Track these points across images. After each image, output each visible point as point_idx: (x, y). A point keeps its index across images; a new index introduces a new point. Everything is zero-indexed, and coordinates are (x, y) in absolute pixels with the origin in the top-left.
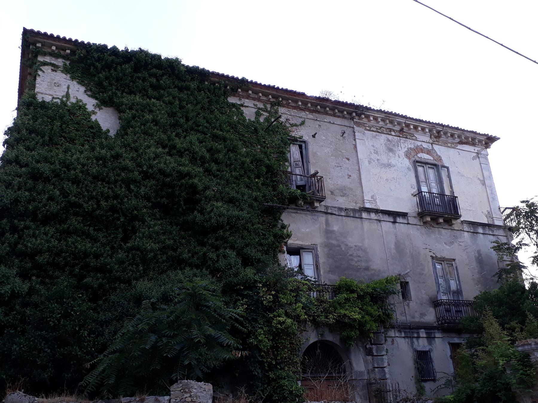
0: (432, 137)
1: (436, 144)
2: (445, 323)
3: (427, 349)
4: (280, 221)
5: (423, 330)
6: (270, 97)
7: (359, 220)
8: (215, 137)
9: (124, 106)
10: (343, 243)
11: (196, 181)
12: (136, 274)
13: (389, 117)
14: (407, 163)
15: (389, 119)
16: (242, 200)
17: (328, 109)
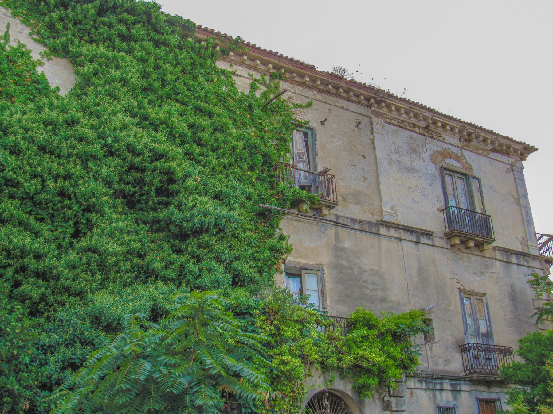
0: (462, 139)
1: (465, 149)
2: (475, 373)
4: (277, 230)
5: (447, 381)
6: (270, 66)
7: (375, 236)
8: (199, 110)
9: (83, 58)
11: (174, 164)
12: (91, 284)
13: (414, 109)
14: (433, 169)
15: (413, 112)
16: (233, 196)
17: (341, 90)
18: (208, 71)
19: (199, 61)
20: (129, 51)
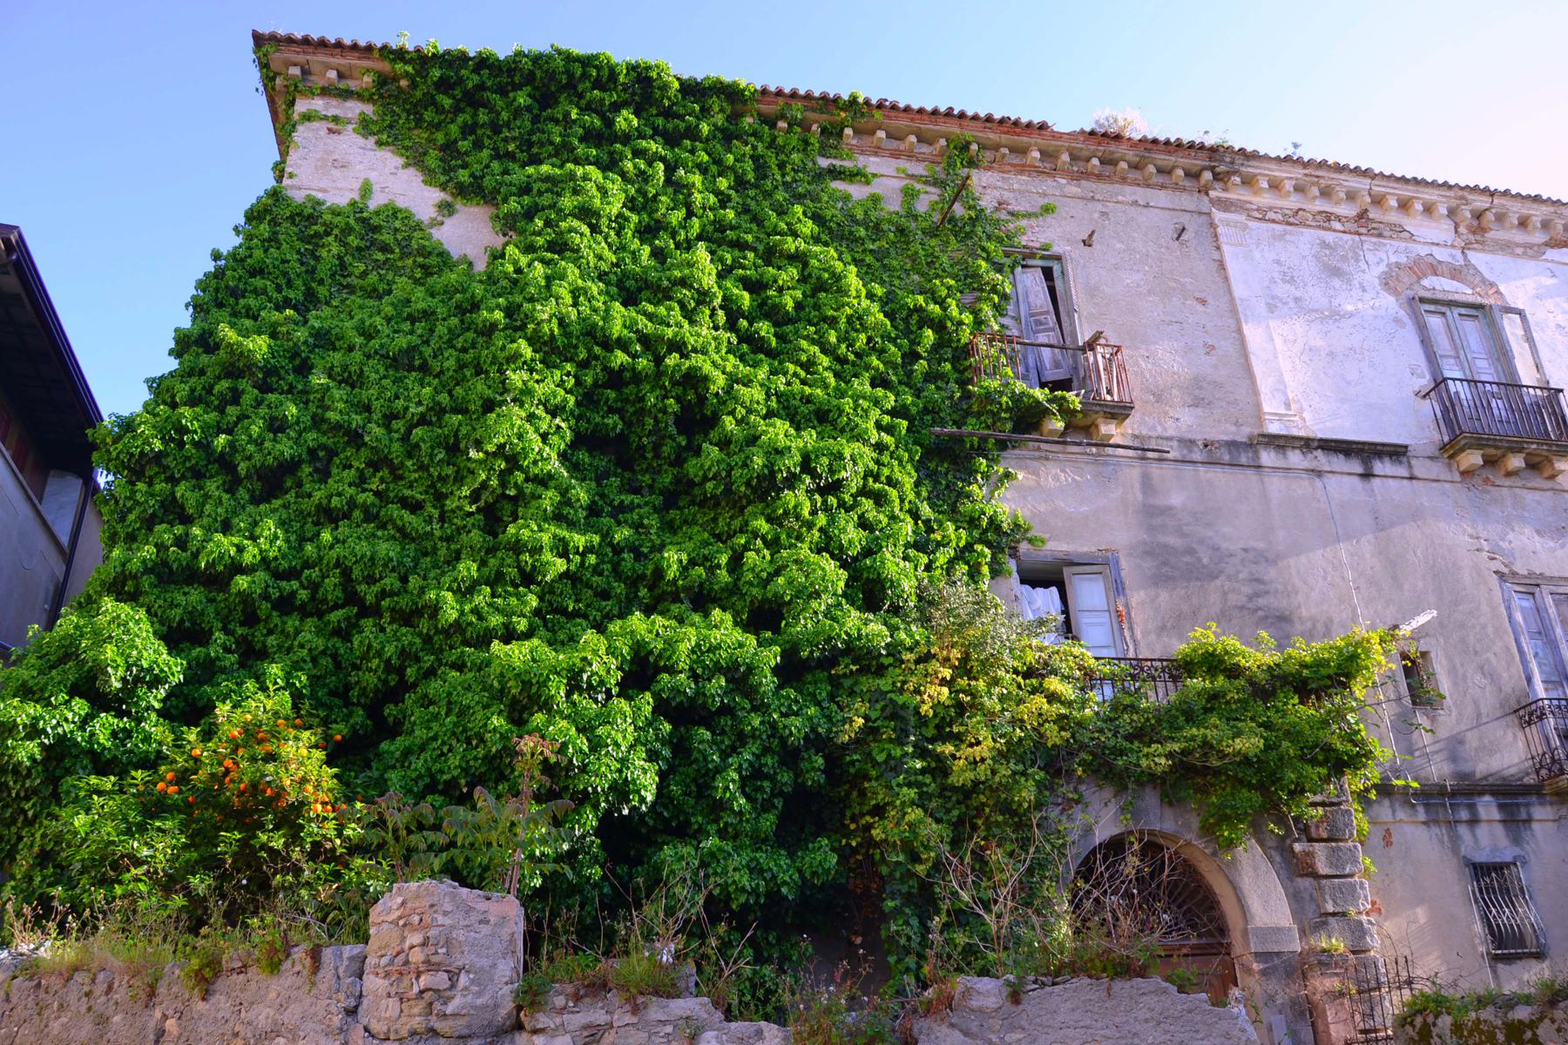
3: (1507, 858)
5: (1487, 798)
7: (1249, 472)
10: (1201, 542)
13: (1319, 176)
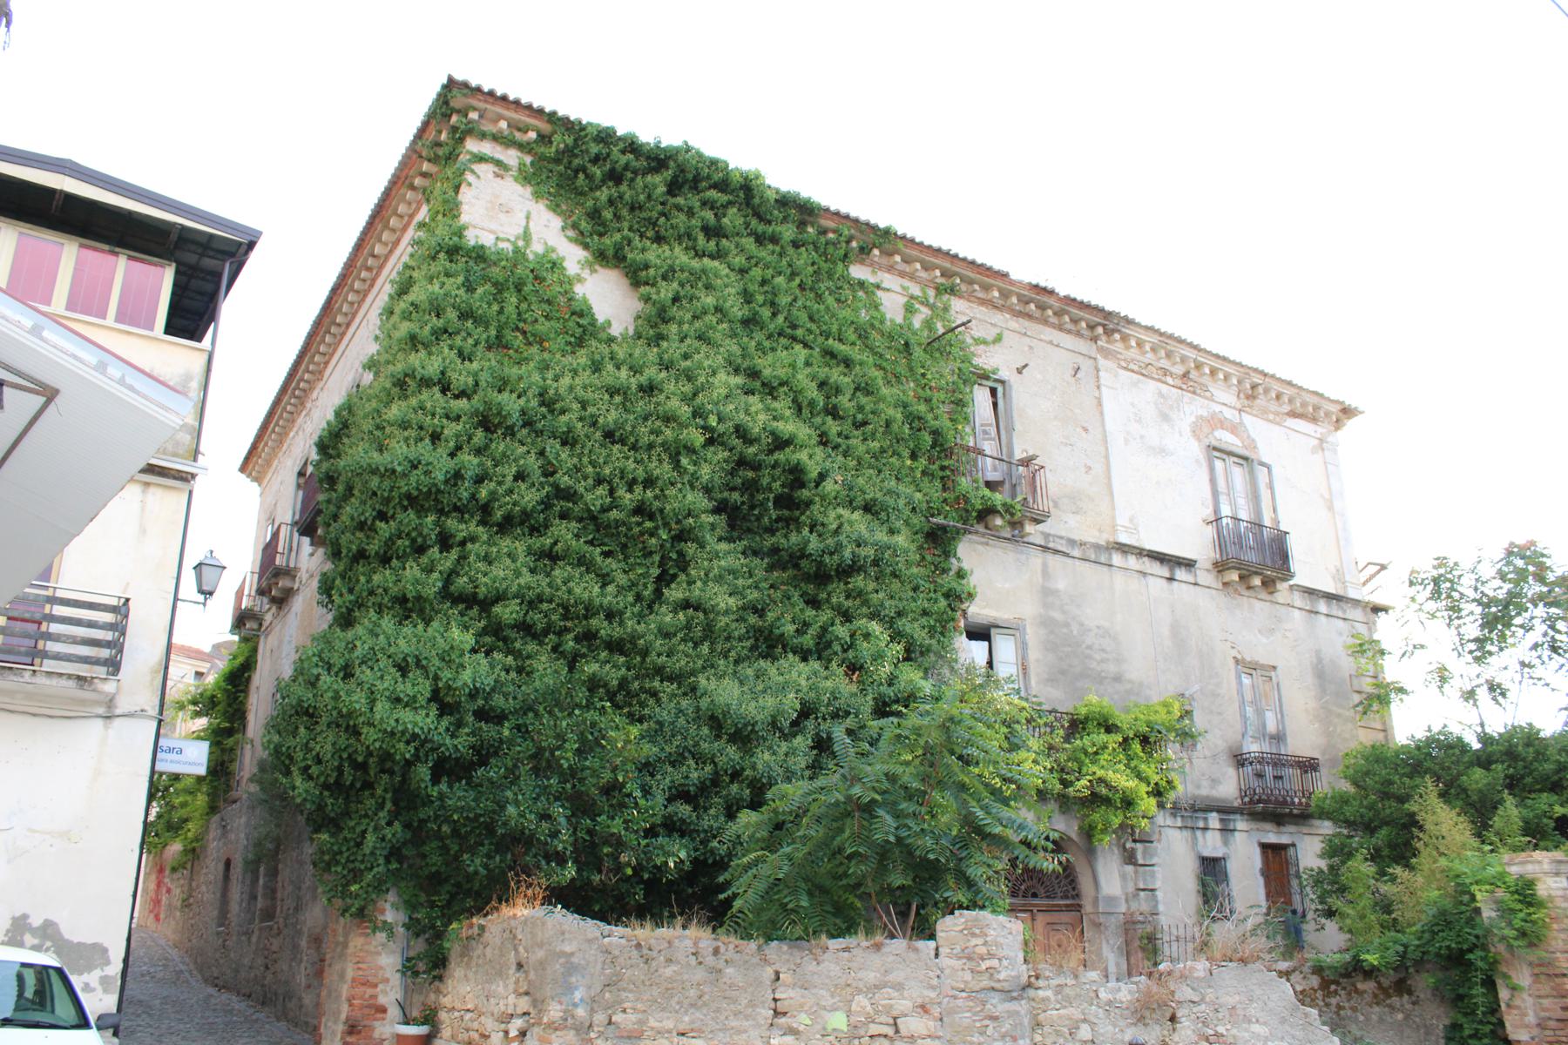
2: (1259, 801)
3: (1220, 855)
5: (1214, 814)
6: (938, 273)
7: (1105, 569)
9: (652, 271)
11: (803, 456)
13: (1167, 342)
14: (1195, 450)
18: (840, 284)
19: (825, 266)
20: (718, 255)
